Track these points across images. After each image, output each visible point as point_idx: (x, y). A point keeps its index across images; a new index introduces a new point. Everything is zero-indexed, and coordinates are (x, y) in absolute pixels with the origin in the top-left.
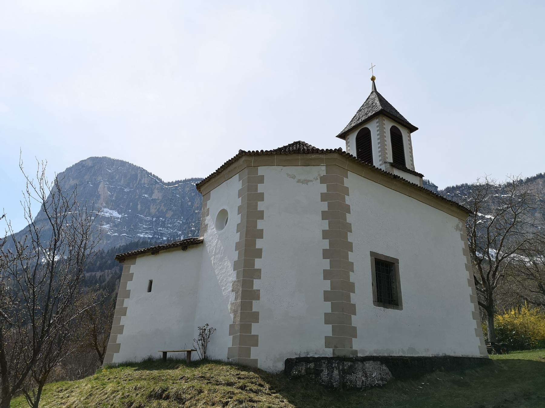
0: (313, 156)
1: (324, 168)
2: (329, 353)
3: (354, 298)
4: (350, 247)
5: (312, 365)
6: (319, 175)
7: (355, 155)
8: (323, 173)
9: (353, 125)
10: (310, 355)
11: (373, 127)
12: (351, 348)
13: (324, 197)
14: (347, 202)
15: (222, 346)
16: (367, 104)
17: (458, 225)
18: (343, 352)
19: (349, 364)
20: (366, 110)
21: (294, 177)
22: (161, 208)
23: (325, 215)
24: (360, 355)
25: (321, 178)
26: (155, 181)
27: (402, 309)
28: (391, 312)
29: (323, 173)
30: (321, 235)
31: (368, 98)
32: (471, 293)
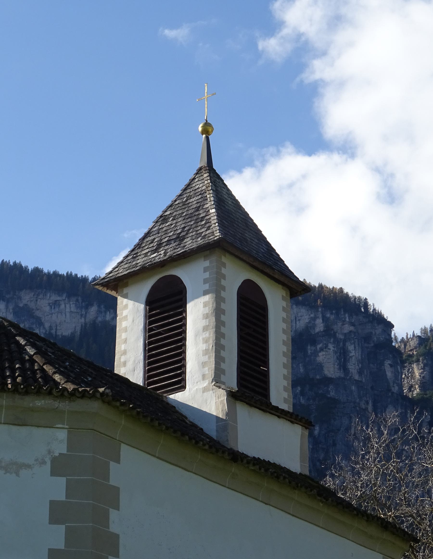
1: (62, 435)
6: (49, 452)
8: (61, 448)
9: (141, 261)
11: (192, 275)
14: (114, 528)
16: (184, 207)
25: (54, 460)
29: (61, 448)
30: (45, 512)
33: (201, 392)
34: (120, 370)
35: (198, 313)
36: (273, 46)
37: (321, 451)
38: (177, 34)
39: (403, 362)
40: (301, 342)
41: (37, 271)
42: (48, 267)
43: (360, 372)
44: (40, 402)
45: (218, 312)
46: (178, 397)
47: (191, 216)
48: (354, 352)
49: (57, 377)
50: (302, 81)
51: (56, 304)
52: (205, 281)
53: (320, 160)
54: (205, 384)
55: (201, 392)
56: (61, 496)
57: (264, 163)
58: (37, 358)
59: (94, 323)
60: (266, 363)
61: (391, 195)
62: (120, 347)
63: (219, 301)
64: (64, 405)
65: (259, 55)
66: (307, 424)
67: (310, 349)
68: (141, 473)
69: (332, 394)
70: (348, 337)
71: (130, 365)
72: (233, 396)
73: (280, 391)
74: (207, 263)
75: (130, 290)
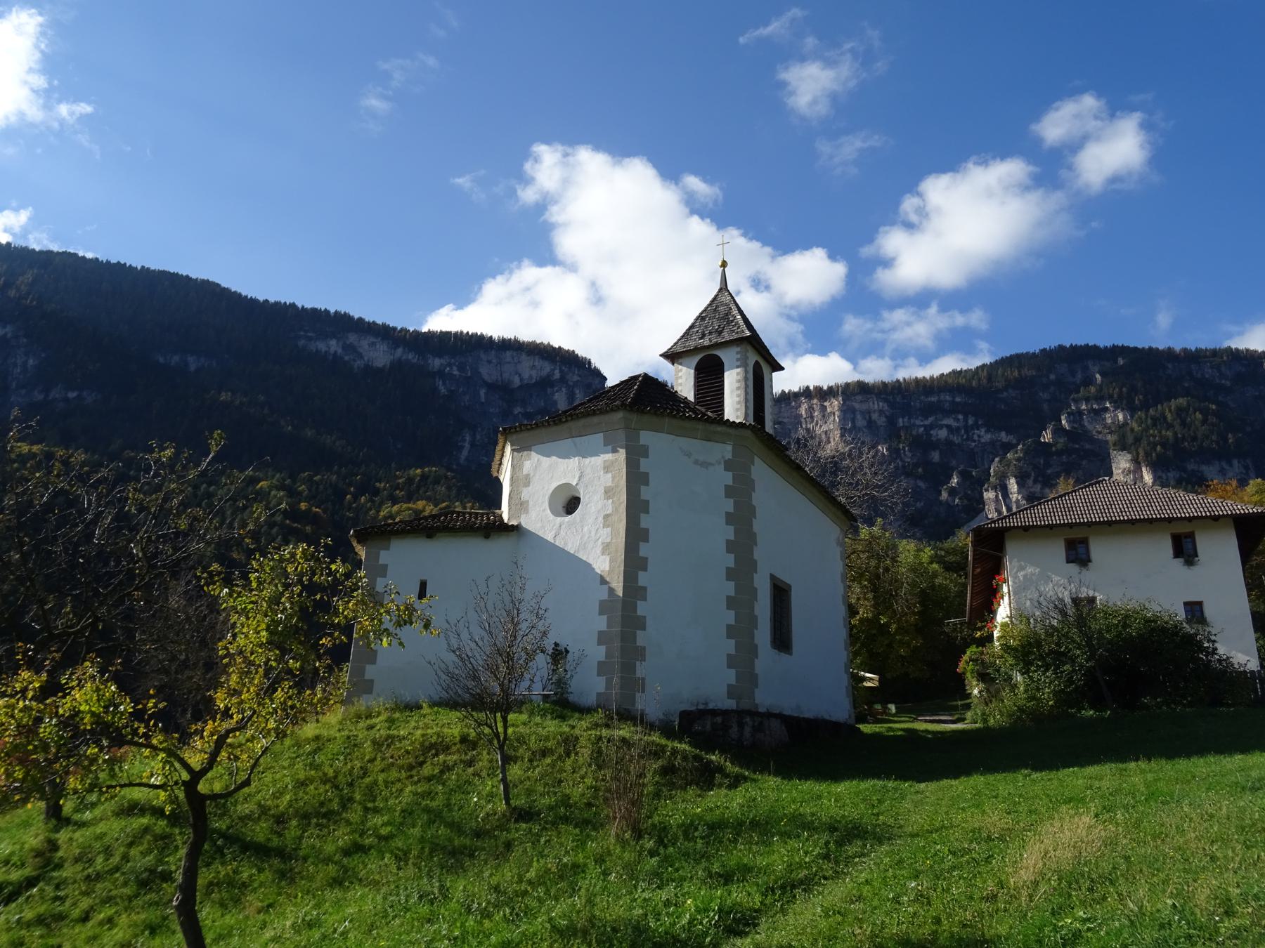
0: (719, 429)
1: (729, 448)
2: (730, 704)
5: (719, 719)
7: (691, 398)
8: (729, 456)
10: (711, 706)
11: (727, 356)
15: (589, 684)
21: (689, 455)
25: (726, 462)
28: (784, 656)
29: (729, 456)
38: (463, 181)
41: (360, 319)
42: (369, 318)
47: (722, 318)
51: (373, 344)
53: (548, 270)
59: (400, 360)
61: (597, 298)
63: (746, 372)
67: (549, 390)
74: (738, 349)
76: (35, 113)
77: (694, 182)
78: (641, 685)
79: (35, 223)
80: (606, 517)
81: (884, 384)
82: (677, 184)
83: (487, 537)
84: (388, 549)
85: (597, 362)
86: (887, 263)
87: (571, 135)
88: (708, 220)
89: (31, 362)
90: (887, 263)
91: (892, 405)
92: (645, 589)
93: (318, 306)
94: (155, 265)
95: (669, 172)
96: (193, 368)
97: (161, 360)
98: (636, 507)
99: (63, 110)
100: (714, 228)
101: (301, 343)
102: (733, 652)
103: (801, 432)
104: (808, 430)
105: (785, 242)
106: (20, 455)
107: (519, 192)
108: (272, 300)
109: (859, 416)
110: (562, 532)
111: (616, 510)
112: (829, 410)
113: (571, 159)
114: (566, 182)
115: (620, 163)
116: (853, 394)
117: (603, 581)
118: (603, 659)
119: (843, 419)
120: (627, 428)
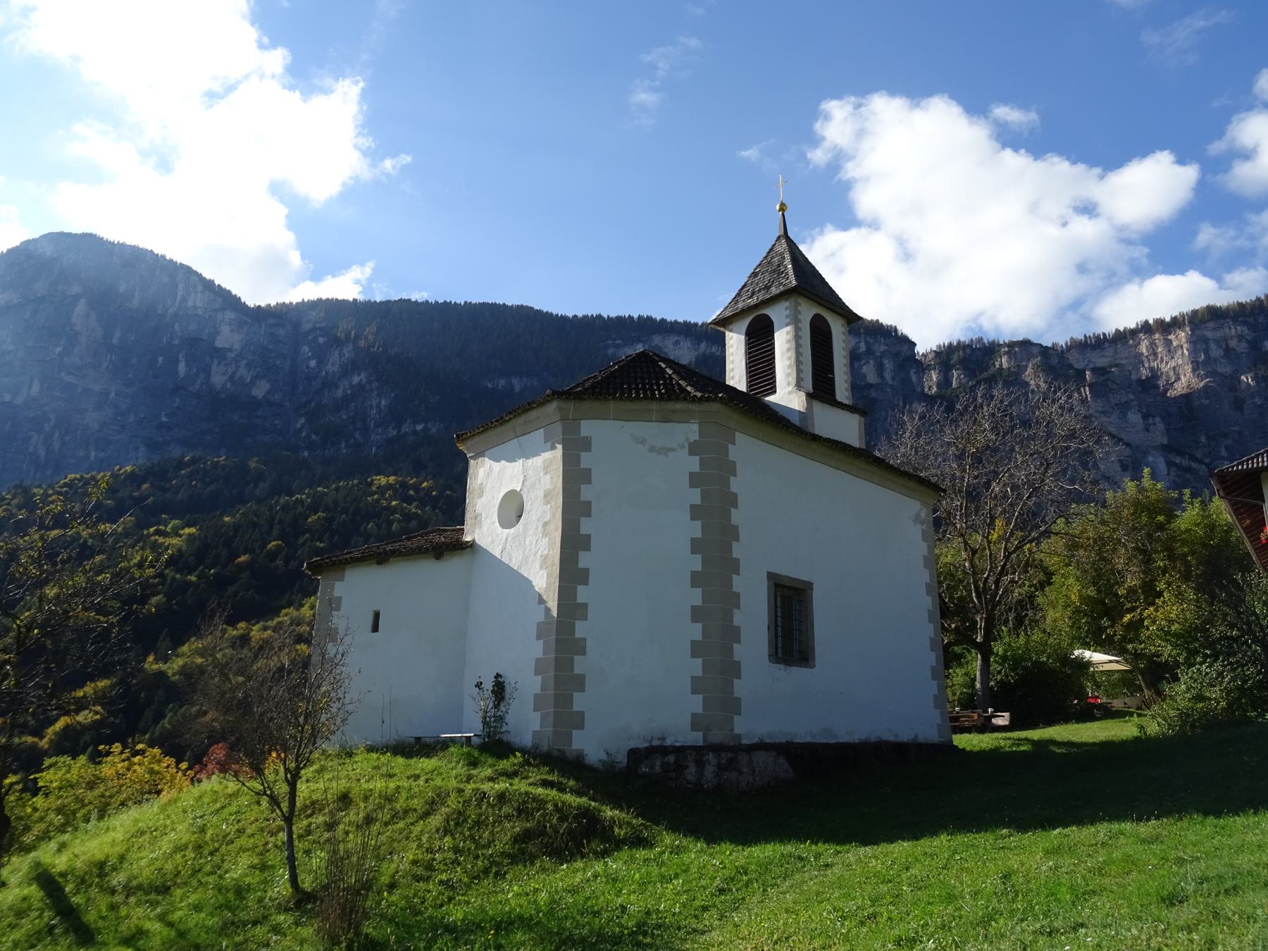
1: (695, 427)
2: (696, 738)
3: (739, 651)
4: (734, 566)
5: (671, 758)
8: (695, 437)
9: (740, 305)
10: (668, 742)
11: (777, 313)
12: (732, 730)
13: (694, 480)
15: (526, 722)
16: (769, 265)
17: (918, 514)
18: (717, 737)
19: (730, 755)
20: (767, 277)
21: (643, 441)
22: (239, 374)
23: (695, 512)
24: (745, 741)
26: (230, 301)
27: (814, 666)
28: (798, 672)
29: (695, 437)
31: (771, 250)
32: (932, 635)
33: (787, 394)
34: (730, 382)
35: (783, 340)
36: (818, 156)
37: (870, 432)
38: (750, 154)
39: (924, 370)
40: (854, 357)
41: (663, 320)
42: (670, 318)
43: (893, 379)
44: (679, 406)
45: (797, 337)
46: (771, 399)
47: (774, 271)
48: (888, 364)
49: (689, 388)
50: (840, 180)
51: (677, 343)
52: (787, 316)
53: (853, 233)
54: (790, 388)
55: (787, 394)
56: (697, 469)
57: (813, 241)
58: (674, 376)
59: (704, 355)
60: (832, 372)
61: (906, 254)
62: (729, 366)
63: (797, 330)
64: (695, 407)
65: (808, 162)
66: (862, 413)
68: (750, 453)
69: (873, 395)
70: (883, 354)
71: (737, 378)
72: (810, 396)
73: (842, 391)
74: (787, 304)
75: (735, 326)
76: (366, 174)
77: (1004, 112)
78: (578, 721)
79: (376, 275)
80: (545, 524)
81: (1240, 305)
82: (986, 117)
83: (380, 562)
84: (342, 579)
85: (905, 329)
86: (1247, 155)
87: (860, 85)
88: (1023, 151)
89: (383, 403)
90: (1247, 155)
91: (1253, 327)
92: (585, 606)
93: (621, 314)
94: (476, 299)
95: (975, 107)
96: (517, 389)
97: (490, 386)
98: (575, 509)
99: (388, 164)
100: (1032, 159)
101: (611, 351)
102: (700, 674)
103: (1145, 373)
104: (1152, 369)
105: (1109, 157)
106: (379, 487)
107: (809, 155)
108: (580, 315)
109: (1213, 346)
110: (508, 547)
111: (554, 515)
112: (1175, 344)
113: (863, 109)
114: (860, 134)
115: (918, 105)
116: (1203, 322)
117: (541, 601)
118: (538, 691)
119: (1194, 352)
120: (564, 419)
